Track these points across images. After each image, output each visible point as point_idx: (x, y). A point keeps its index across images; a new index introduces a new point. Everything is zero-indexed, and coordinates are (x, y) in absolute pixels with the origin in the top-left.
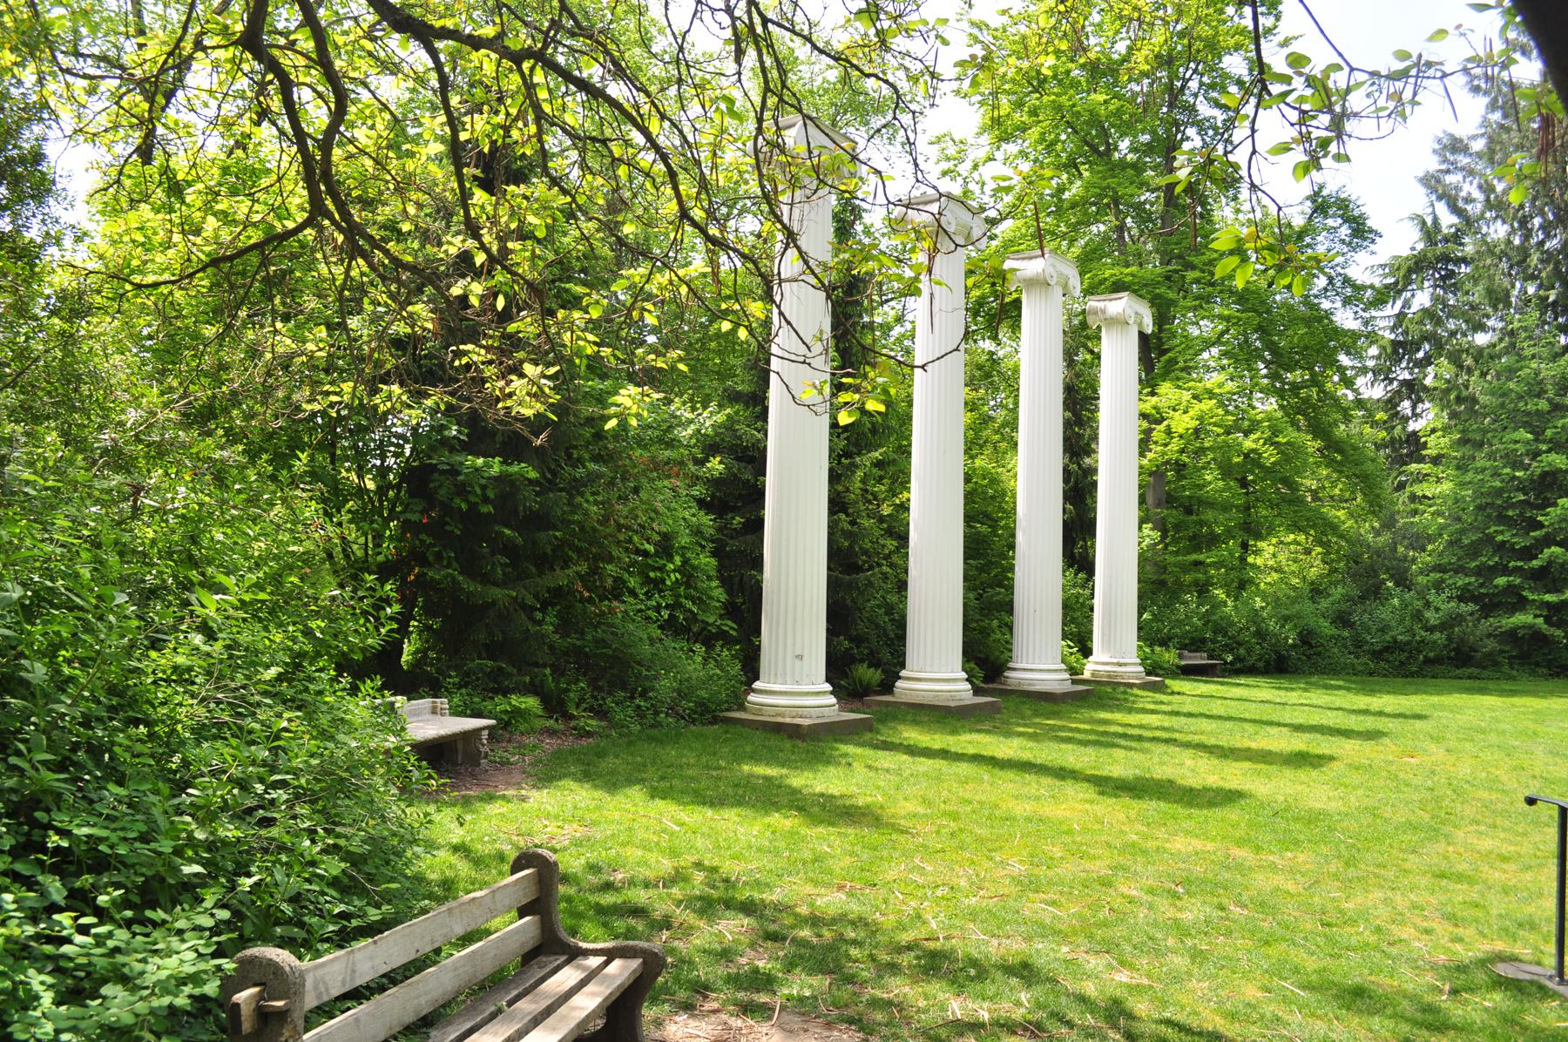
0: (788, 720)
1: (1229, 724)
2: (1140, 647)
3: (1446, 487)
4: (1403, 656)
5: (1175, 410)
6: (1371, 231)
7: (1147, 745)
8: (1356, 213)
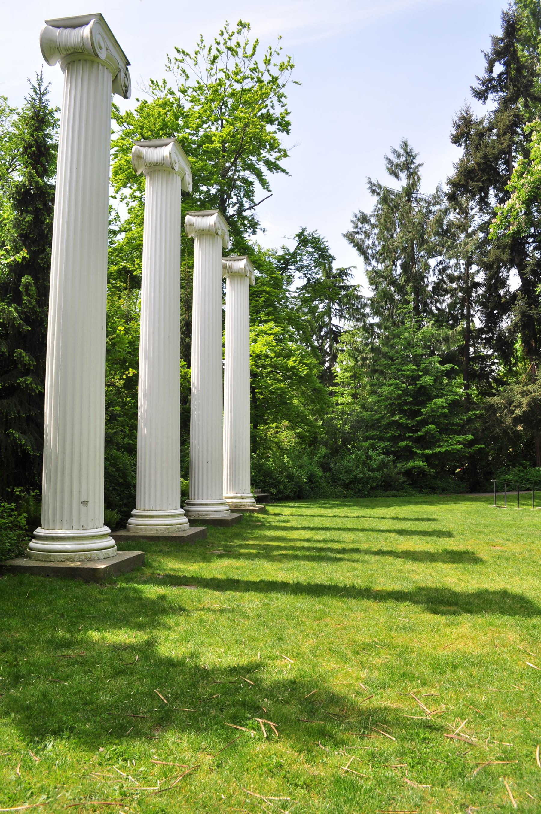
0: (78, 564)
4: (360, 486)
6: (331, 256)
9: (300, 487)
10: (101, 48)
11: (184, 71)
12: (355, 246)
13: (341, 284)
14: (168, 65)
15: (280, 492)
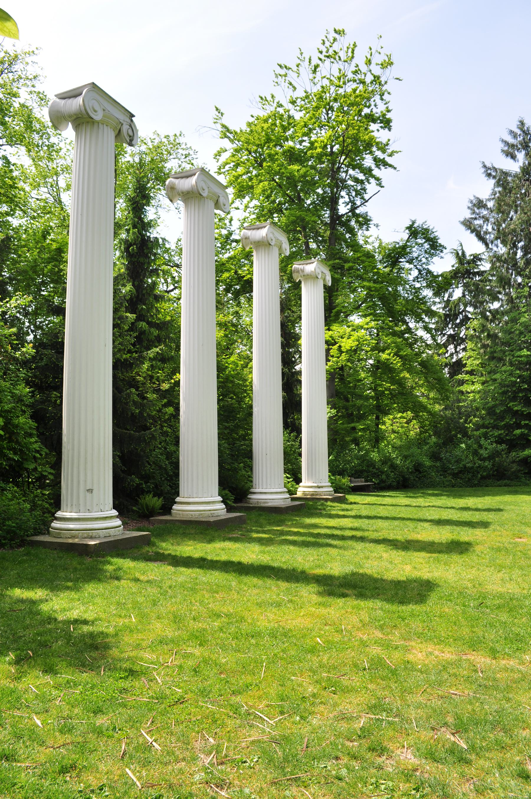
0: (76, 541)
1: (396, 523)
2: (329, 476)
3: (478, 387)
4: (470, 475)
5: (342, 338)
6: (441, 246)
7: (350, 543)
8: (432, 236)
9: (403, 477)
10: (95, 111)
11: (291, 84)
12: (472, 232)
13: (476, 270)
14: (276, 80)
15: (382, 481)
